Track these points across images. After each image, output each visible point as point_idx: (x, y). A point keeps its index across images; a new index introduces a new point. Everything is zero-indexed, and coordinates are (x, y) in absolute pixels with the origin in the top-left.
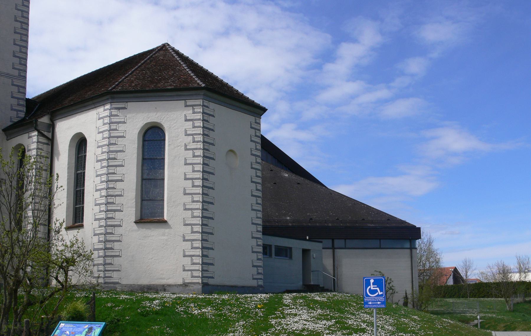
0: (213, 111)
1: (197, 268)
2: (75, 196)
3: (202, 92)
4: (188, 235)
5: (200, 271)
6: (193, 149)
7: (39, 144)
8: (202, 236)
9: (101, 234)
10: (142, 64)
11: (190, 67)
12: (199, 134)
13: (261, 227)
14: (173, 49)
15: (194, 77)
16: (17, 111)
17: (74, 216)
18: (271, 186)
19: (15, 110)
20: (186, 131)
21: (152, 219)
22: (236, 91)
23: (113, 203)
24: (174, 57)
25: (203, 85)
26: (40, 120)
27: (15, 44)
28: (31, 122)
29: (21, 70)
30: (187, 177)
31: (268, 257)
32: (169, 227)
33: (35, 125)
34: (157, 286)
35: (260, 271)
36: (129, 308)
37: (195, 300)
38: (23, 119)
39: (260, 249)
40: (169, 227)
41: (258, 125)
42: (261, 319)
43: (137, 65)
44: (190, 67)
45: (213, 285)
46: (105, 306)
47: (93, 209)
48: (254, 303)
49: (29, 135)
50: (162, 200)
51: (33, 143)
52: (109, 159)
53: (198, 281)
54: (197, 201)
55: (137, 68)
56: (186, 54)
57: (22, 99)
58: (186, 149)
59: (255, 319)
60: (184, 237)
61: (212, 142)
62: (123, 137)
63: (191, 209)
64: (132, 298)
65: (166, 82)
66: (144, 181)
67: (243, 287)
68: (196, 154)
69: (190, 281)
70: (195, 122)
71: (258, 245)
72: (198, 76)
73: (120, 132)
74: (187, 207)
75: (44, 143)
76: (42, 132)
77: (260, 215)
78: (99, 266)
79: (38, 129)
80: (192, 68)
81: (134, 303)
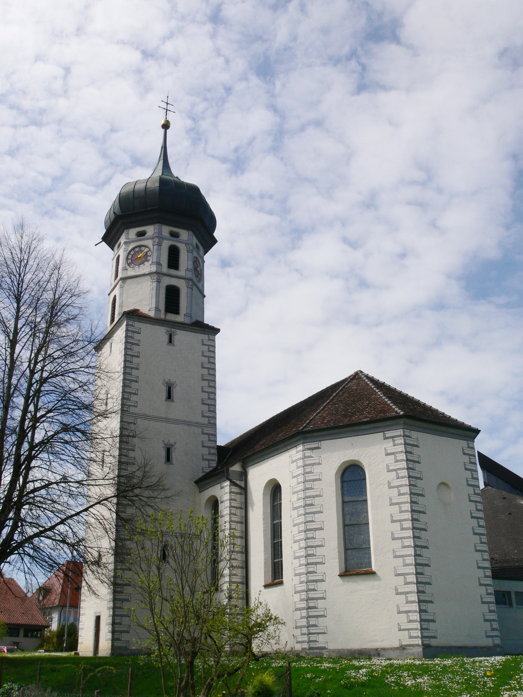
0: (416, 440)
1: (415, 627)
2: (273, 550)
3: (401, 421)
4: (401, 587)
5: (419, 630)
6: (398, 487)
7: (231, 494)
8: (417, 587)
9: (302, 591)
10: (334, 397)
11: (387, 394)
12: (403, 469)
13: (489, 570)
14: (367, 376)
15: (391, 405)
16: (209, 460)
17: (273, 571)
18: (505, 518)
19: (206, 460)
20: (388, 466)
21: (358, 570)
22: (442, 414)
23: (313, 555)
24: (368, 385)
25: (402, 413)
26: (230, 469)
27: (203, 391)
28: (223, 471)
29: (210, 417)
30: (394, 519)
31: (508, 606)
32: (379, 579)
33: (226, 474)
34: (370, 650)
35: (494, 626)
36: (331, 680)
37: (409, 668)
38: (215, 469)
39: (492, 599)
40: (379, 579)
41: (472, 450)
42: (490, 691)
43: (329, 398)
44: (387, 394)
45: (437, 647)
46: (304, 678)
47: (292, 563)
48: (483, 669)
49: (221, 485)
50: (368, 547)
51: (226, 493)
52: (306, 505)
53: (417, 642)
54: (408, 547)
55: (329, 403)
56: (382, 380)
57: (213, 448)
58: (390, 487)
59: (483, 691)
60: (396, 589)
61: (419, 476)
62: (319, 480)
63: (402, 556)
64: (335, 667)
65: (361, 415)
66: (346, 528)
67: (475, 648)
68: (402, 492)
69: (408, 643)
70: (397, 455)
71: (488, 594)
72: (397, 402)
73: (315, 474)
74: (398, 554)
75: (237, 493)
76: (235, 481)
77: (486, 556)
78: (302, 629)
79: (230, 478)
80: (389, 394)
81: (337, 673)
